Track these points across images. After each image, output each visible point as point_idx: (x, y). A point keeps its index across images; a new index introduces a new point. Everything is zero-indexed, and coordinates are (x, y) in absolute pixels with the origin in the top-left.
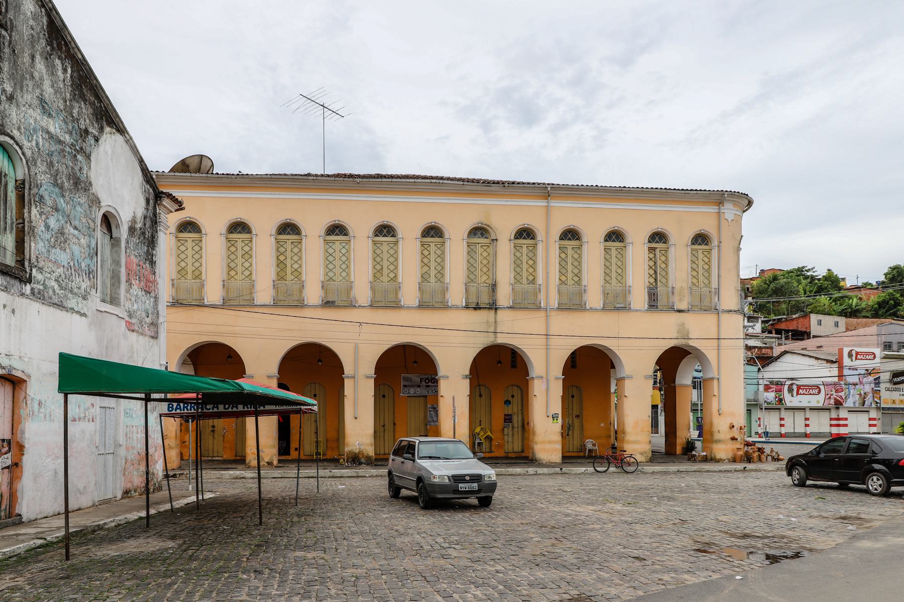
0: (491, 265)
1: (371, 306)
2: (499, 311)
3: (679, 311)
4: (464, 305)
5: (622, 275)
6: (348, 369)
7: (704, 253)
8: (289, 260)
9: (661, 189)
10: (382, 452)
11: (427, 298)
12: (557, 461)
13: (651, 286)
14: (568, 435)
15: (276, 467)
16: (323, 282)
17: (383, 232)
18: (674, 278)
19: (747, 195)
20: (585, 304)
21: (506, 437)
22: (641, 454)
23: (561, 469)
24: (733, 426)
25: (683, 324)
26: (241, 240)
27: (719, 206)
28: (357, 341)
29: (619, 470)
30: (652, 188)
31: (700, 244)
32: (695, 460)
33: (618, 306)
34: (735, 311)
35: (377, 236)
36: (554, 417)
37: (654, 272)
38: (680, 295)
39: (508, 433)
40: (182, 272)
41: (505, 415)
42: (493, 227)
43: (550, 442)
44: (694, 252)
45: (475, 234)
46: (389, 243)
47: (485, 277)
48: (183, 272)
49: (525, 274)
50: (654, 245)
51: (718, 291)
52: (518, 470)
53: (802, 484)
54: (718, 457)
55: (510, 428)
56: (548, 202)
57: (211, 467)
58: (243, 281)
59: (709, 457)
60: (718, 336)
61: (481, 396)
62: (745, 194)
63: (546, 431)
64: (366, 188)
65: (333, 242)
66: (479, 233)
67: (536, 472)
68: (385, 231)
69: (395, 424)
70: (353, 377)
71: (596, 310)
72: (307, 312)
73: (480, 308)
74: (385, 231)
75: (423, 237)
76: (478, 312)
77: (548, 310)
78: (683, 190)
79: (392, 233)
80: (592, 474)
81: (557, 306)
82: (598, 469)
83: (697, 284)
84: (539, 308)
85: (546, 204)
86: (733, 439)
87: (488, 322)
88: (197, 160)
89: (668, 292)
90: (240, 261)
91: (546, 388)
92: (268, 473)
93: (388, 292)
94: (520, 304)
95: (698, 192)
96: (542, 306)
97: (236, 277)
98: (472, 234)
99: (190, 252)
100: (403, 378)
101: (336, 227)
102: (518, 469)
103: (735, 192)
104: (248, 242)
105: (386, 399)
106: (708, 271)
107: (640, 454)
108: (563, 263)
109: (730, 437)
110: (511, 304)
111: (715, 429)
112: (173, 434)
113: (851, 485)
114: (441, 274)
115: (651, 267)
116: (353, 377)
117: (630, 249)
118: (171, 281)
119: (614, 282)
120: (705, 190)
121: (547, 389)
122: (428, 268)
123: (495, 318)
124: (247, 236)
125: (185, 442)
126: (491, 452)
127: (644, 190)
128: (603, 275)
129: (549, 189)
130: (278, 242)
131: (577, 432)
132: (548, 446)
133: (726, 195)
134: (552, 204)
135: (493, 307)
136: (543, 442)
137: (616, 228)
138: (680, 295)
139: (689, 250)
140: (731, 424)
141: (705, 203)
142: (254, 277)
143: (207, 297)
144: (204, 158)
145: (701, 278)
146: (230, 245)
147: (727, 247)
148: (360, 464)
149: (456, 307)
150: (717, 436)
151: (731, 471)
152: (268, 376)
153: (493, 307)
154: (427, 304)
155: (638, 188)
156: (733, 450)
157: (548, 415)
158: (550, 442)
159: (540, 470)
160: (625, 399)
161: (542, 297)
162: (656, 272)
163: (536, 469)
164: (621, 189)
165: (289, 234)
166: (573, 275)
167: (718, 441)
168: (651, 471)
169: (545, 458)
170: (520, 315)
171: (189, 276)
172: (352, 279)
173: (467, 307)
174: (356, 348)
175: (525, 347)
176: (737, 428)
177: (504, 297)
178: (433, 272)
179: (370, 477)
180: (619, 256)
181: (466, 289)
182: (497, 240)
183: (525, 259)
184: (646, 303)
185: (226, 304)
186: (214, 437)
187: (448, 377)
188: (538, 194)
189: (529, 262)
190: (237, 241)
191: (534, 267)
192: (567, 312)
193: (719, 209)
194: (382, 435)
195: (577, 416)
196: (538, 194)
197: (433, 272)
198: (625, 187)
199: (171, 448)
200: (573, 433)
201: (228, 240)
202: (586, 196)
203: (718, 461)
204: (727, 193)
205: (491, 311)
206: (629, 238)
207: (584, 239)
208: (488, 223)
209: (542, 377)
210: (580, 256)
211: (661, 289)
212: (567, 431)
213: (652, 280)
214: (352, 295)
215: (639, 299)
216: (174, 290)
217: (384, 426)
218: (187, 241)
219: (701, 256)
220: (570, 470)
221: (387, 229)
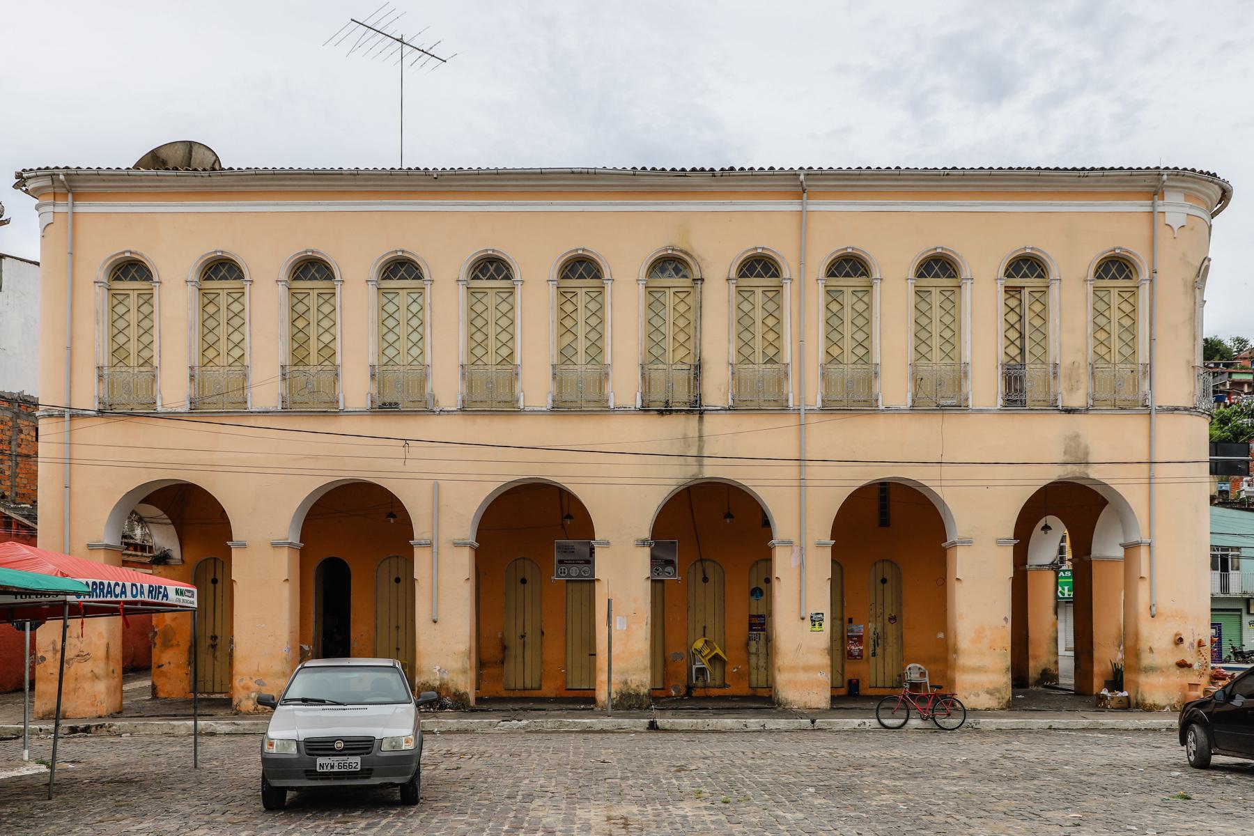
0: (693, 327)
1: (463, 410)
3: (1069, 411)
4: (639, 406)
5: (952, 343)
6: (421, 530)
7: (1098, 293)
8: (313, 326)
9: (1029, 169)
10: (520, 685)
11: (569, 394)
12: (820, 706)
13: (1013, 362)
14: (874, 655)
16: (373, 367)
17: (489, 270)
18: (1057, 344)
19: (1215, 175)
20: (877, 400)
21: (753, 659)
22: (990, 693)
23: (813, 722)
24: (1181, 640)
25: (1076, 437)
26: (226, 291)
27: (1152, 199)
29: (929, 724)
30: (1010, 168)
31: (1114, 277)
32: (1105, 707)
33: (943, 402)
34: (1186, 409)
35: (476, 278)
36: (816, 620)
37: (1017, 335)
38: (1070, 379)
39: (757, 650)
40: (118, 353)
41: (751, 616)
42: (694, 255)
43: (807, 669)
44: (1101, 294)
45: (663, 271)
46: (498, 291)
47: (681, 353)
48: (123, 354)
49: (758, 344)
50: (1017, 282)
51: (1149, 369)
52: (728, 722)
53: (1202, 763)
54: (1149, 701)
55: (762, 642)
56: (802, 204)
57: (184, 712)
58: (499, 367)
59: (1133, 701)
61: (705, 580)
62: (1208, 173)
63: (800, 646)
64: (452, 189)
65: (396, 291)
66: (670, 267)
67: (764, 726)
68: (492, 269)
69: (543, 633)
70: (430, 545)
71: (898, 411)
72: (345, 425)
73: (671, 412)
74: (492, 269)
75: (564, 278)
76: (668, 420)
77: (802, 412)
78: (1074, 169)
79: (506, 271)
80: (874, 731)
81: (819, 404)
82: (887, 722)
83: (1107, 357)
84: (784, 409)
85: (798, 208)
86: (1182, 665)
87: (685, 438)
88: (180, 152)
89: (1046, 373)
90: (223, 331)
91: (797, 563)
92: (257, 724)
93: (763, 380)
94: (748, 403)
95: (1106, 173)
96: (791, 404)
97: (216, 361)
98: (657, 269)
99: (581, 315)
100: (559, 547)
101: (221, 264)
102: (729, 721)
103: (1185, 169)
104: (239, 295)
105: (528, 585)
106: (1132, 330)
107: (987, 692)
108: (835, 322)
110: (731, 402)
111: (1144, 646)
112: (102, 652)
114: (596, 348)
115: (1012, 326)
116: (430, 545)
117: (967, 288)
118: (96, 371)
119: (936, 355)
120: (1121, 168)
121: (802, 566)
122: (571, 337)
123: (700, 430)
124: (595, 282)
125: (162, 665)
126: (724, 686)
128: (912, 342)
129: (802, 177)
130: (293, 294)
131: (891, 649)
132: (802, 677)
133: (1165, 177)
134: (78, 209)
135: (696, 408)
136: (794, 669)
137: (939, 250)
138: (1070, 379)
139: (1090, 289)
140: (1176, 635)
141: (1123, 195)
142: (247, 361)
143: (162, 398)
144: (195, 148)
145: (1116, 344)
146: (115, 302)
147: (1172, 282)
148: (443, 707)
149: (623, 411)
150: (1147, 660)
151: (1160, 730)
152: (272, 544)
153: (696, 408)
154: (569, 404)
155: (981, 168)
156: (1183, 687)
157: (803, 615)
158: (807, 669)
159: (782, 723)
160: (957, 585)
161: (791, 388)
162: (1022, 336)
163: (762, 721)
164: (947, 171)
165: (313, 278)
166: (855, 344)
167: (1151, 669)
168: (994, 727)
169: (797, 698)
170: (748, 423)
171: (133, 361)
172: (428, 361)
173: (645, 409)
174: (437, 490)
175: (1114, 482)
176: (1192, 644)
177: (716, 389)
178: (582, 345)
179: (442, 733)
180: (947, 305)
181: (643, 374)
182: (702, 280)
183: (759, 315)
184: (1000, 396)
185: (198, 410)
186: (215, 657)
187: (608, 543)
188: (783, 189)
189: (767, 321)
190: (128, 295)
191: (777, 330)
192: (843, 416)
193: (1153, 205)
194: (520, 654)
195: (893, 619)
196: (783, 189)
197: (582, 345)
198: (954, 168)
199: (97, 678)
200: (884, 650)
201: (203, 293)
202: (878, 189)
203: (1150, 709)
204: (1165, 172)
205: (691, 416)
206: (967, 268)
207: (876, 274)
208: (685, 247)
209: (792, 543)
210: (869, 307)
211: (1033, 371)
212: (871, 648)
213: (1014, 351)
214: (428, 390)
216: (104, 386)
217: (523, 636)
218: (128, 295)
219: (1115, 299)
220: (829, 723)
221: (495, 265)
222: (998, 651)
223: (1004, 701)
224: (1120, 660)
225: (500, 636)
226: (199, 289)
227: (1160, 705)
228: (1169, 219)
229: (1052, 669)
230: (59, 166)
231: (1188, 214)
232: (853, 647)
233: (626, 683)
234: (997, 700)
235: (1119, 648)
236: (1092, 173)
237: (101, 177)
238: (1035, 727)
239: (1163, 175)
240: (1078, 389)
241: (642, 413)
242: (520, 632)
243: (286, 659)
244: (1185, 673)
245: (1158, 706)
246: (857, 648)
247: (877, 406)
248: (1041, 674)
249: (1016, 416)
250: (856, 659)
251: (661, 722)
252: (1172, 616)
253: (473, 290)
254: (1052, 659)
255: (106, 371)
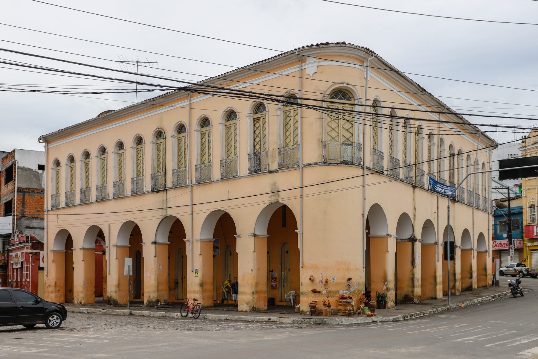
2: (168, 192)
6: (188, 235)
15: (83, 305)
22: (247, 304)
25: (275, 184)
28: (110, 223)
34: (316, 164)
38: (272, 156)
60: (192, 202)
84: (186, 186)
109: (312, 289)
113: (37, 326)
123: (166, 197)
127: (270, 60)
149: (216, 181)
215: (244, 167)
220: (169, 314)
222: (249, 284)
223: (251, 308)
224: (385, 290)
225: (174, 278)
226: (225, 126)
227: (305, 311)
228: (308, 71)
229: (410, 295)
230: (228, 71)
231: (317, 66)
232: (273, 283)
233: (149, 297)
234: (249, 307)
235: (385, 283)
236: (270, 60)
237: (277, 60)
238: (222, 318)
239: (296, 52)
240: (275, 161)
241: (152, 193)
242: (181, 277)
243: (83, 287)
244: (317, 295)
245: (304, 312)
246: (275, 283)
247: (74, 204)
248: (404, 298)
249: (254, 177)
250: (274, 288)
251: (133, 312)
252: (310, 267)
253: (285, 112)
254: (410, 289)
255: (283, 150)
